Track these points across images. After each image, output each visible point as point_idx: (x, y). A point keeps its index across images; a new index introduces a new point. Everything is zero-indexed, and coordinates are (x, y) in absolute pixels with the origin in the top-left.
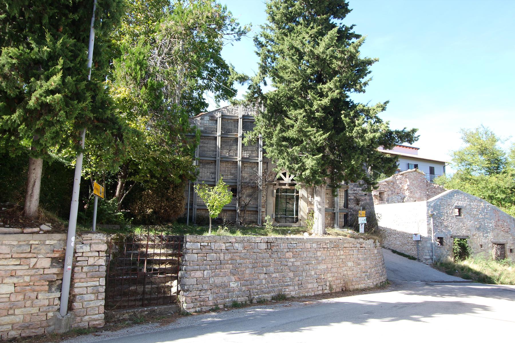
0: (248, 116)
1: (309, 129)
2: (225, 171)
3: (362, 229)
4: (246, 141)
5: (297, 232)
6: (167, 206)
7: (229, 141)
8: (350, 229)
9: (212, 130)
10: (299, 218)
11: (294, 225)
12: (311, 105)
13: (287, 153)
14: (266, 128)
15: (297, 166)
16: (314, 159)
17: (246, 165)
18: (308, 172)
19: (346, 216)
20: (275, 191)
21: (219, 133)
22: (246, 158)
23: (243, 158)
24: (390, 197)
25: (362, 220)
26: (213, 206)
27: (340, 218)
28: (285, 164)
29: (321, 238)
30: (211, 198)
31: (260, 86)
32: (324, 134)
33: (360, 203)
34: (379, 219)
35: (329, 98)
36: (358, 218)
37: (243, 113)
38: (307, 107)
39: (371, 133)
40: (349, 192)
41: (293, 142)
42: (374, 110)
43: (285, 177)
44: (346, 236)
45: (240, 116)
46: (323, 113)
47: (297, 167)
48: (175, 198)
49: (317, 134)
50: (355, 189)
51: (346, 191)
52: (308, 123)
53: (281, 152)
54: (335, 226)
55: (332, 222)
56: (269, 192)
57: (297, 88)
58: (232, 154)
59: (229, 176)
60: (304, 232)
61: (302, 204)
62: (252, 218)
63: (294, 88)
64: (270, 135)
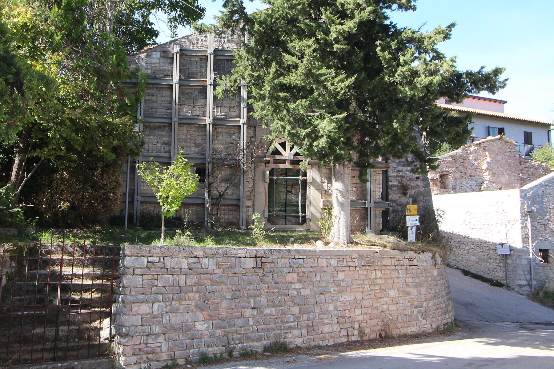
0: (223, 50)
1: (324, 70)
2: (185, 141)
3: (412, 236)
4: (220, 91)
5: (304, 240)
6: (93, 198)
7: (193, 92)
8: (393, 235)
9: (165, 73)
12: (327, 32)
13: (288, 110)
14: (252, 70)
15: (304, 132)
16: (333, 121)
17: (219, 130)
18: (322, 142)
19: (385, 214)
20: (268, 173)
21: (176, 79)
22: (220, 119)
24: (458, 182)
25: (412, 221)
26: (168, 197)
27: (375, 217)
29: (345, 249)
30: (164, 184)
32: (347, 78)
33: (409, 191)
34: (440, 219)
35: (356, 20)
36: (405, 216)
37: (215, 46)
38: (320, 35)
39: (426, 76)
40: (391, 174)
41: (297, 93)
42: (430, 38)
44: (385, 246)
45: (210, 51)
46: (347, 44)
47: (304, 133)
48: (106, 185)
49: (336, 80)
50: (399, 170)
51: (385, 173)
53: (277, 109)
54: (368, 230)
55: (362, 224)
57: (304, 4)
58: (197, 113)
59: (193, 149)
60: (316, 239)
61: (312, 192)
62: (230, 217)
64: (259, 82)
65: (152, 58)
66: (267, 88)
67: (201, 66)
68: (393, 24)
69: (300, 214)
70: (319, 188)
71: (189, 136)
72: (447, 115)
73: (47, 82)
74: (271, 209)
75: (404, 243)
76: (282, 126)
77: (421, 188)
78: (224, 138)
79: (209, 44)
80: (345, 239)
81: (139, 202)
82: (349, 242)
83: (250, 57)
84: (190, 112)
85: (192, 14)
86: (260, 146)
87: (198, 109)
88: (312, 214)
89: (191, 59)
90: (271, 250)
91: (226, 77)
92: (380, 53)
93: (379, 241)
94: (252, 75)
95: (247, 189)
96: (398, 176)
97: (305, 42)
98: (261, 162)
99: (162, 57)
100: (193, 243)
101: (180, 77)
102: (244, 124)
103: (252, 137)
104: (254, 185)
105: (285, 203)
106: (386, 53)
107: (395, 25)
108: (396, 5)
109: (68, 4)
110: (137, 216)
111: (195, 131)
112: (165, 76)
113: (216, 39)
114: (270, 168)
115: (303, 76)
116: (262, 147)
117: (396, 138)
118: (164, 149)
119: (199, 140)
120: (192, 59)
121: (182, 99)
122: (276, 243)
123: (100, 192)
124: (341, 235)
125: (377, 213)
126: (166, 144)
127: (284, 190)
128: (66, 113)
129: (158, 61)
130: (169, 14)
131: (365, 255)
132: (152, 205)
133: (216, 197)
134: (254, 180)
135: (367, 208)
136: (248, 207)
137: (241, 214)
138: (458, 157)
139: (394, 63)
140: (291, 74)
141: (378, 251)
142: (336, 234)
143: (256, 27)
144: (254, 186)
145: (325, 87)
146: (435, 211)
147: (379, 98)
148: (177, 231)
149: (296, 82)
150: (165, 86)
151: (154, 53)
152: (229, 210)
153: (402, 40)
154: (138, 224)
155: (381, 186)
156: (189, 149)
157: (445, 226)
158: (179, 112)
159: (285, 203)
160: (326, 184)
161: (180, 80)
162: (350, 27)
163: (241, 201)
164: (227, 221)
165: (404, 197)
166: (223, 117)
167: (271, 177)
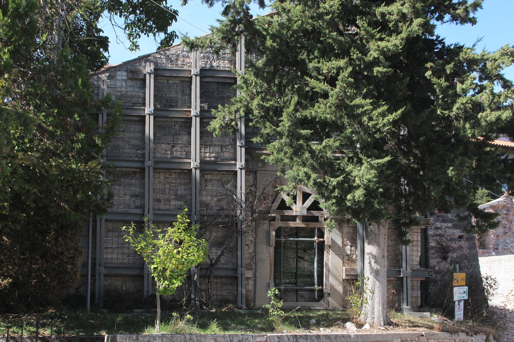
0: (212, 69)
2: (163, 192)
3: (459, 313)
4: (217, 126)
5: (327, 321)
6: (45, 271)
7: (171, 126)
8: (436, 312)
9: (134, 100)
10: (325, 291)
11: (316, 306)
12: (364, 51)
13: (312, 152)
14: (263, 99)
15: (334, 181)
17: (208, 177)
18: (359, 194)
19: (425, 285)
20: (274, 233)
21: (149, 109)
22: (210, 163)
23: (203, 162)
24: (501, 240)
25: (460, 293)
26: (165, 269)
27: (412, 289)
28: (309, 177)
29: (384, 333)
30: (160, 252)
31: (248, 9)
32: (390, 111)
33: (450, 255)
34: (491, 291)
35: (404, 35)
37: (201, 64)
38: (355, 54)
39: (492, 110)
40: (430, 232)
41: (322, 129)
42: (495, 60)
44: (431, 328)
45: (194, 71)
46: (389, 67)
47: (334, 183)
48: (62, 253)
49: (375, 113)
50: (445, 228)
51: (424, 232)
53: (297, 152)
54: (404, 306)
55: (396, 298)
56: (261, 235)
57: (333, 13)
58: (178, 154)
59: (173, 203)
60: (345, 321)
61: (331, 259)
62: (224, 293)
63: (327, 14)
64: (273, 114)
65: (116, 80)
66: (286, 123)
67: (183, 91)
68: (440, 39)
70: (340, 252)
72: (507, 156)
73: (25, 121)
74: (277, 281)
75: (452, 323)
76: (306, 173)
77: (465, 250)
78: (215, 188)
79: (194, 63)
80: (382, 319)
81: (102, 275)
82: (386, 323)
83: (259, 81)
84: (169, 152)
85: (159, 18)
86: (262, 197)
87: (179, 149)
89: (170, 83)
90: (296, 336)
91: (224, 107)
93: (421, 321)
94: (262, 105)
95: (246, 255)
100: (195, 330)
101: (154, 106)
103: (252, 186)
104: (255, 250)
105: (296, 273)
107: (442, 40)
108: (450, 16)
109: (16, 9)
111: (175, 179)
112: (134, 104)
114: (277, 227)
115: (333, 108)
116: (265, 199)
117: (449, 188)
118: (134, 202)
119: (181, 191)
120: (170, 82)
122: (299, 328)
124: (375, 314)
126: (137, 196)
128: (19, 157)
129: (124, 84)
130: (127, 18)
131: (409, 339)
132: (119, 278)
133: (205, 266)
135: (402, 278)
136: (248, 278)
137: (240, 288)
138: (500, 208)
141: (423, 333)
142: (369, 313)
143: (269, 43)
144: (255, 251)
145: (361, 123)
146: (484, 279)
148: (174, 314)
149: (325, 115)
151: (119, 73)
153: (461, 63)
154: (102, 305)
155: (419, 249)
156: (168, 203)
157: (495, 301)
158: (154, 153)
159: (296, 273)
160: (349, 247)
161: (155, 110)
162: (395, 45)
163: (239, 272)
165: (444, 262)
166: (213, 159)
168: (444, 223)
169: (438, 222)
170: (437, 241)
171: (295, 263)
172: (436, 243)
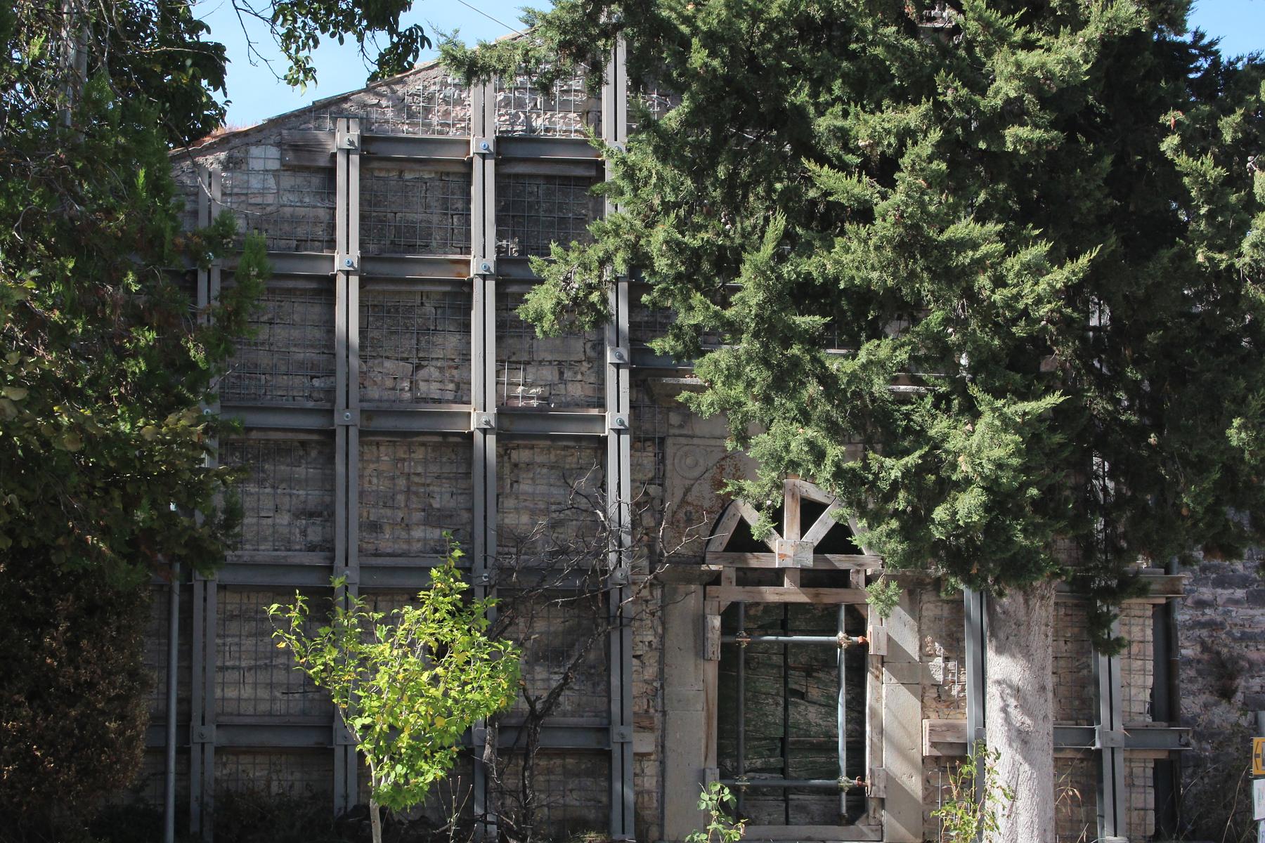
0: (530, 138)
1: (964, 227)
2: (388, 501)
4: (548, 305)
7: (414, 304)
9: (301, 231)
10: (871, 792)
12: (978, 80)
13: (828, 380)
14: (681, 226)
15: (895, 468)
16: (1007, 424)
17: (522, 456)
18: (969, 504)
19: (1166, 775)
20: (717, 622)
21: (346, 256)
22: (526, 414)
23: (504, 412)
26: (394, 731)
27: (1130, 785)
30: (382, 680)
32: (1056, 258)
33: (1241, 682)
35: (1093, 31)
36: (1248, 784)
37: (497, 122)
40: (1182, 616)
43: (804, 528)
45: (479, 143)
46: (1053, 125)
48: (91, 685)
49: (1013, 264)
51: (1164, 614)
52: (953, 192)
53: (784, 379)
56: (680, 632)
58: (433, 390)
59: (418, 533)
61: (886, 696)
62: (573, 800)
65: (249, 172)
66: (749, 294)
67: (445, 201)
68: (1205, 41)
69: (844, 780)
70: (913, 676)
71: (402, 483)
74: (728, 763)
76: (811, 443)
78: (541, 489)
81: (209, 751)
83: (669, 172)
84: (406, 385)
86: (681, 515)
87: (436, 374)
88: (890, 780)
91: (567, 249)
92: (1183, 161)
94: (678, 244)
96: (1198, 624)
97: (893, 118)
98: (689, 582)
99: (287, 168)
102: (619, 432)
104: (661, 671)
105: (783, 740)
106: (1208, 160)
107: (1212, 43)
110: (203, 805)
111: (425, 462)
112: (302, 243)
113: (501, 96)
114: (725, 603)
115: (889, 253)
116: (689, 521)
118: (304, 533)
119: (442, 498)
120: (408, 176)
121: (374, 334)
123: (66, 715)
125: (1137, 771)
126: (311, 515)
127: (779, 686)
129: (271, 182)
132: (259, 759)
133: (513, 721)
134: (662, 651)
135: (1099, 752)
136: (641, 756)
137: (617, 786)
139: (1233, 198)
140: (839, 241)
143: (698, 57)
145: (971, 295)
147: (1166, 329)
149: (863, 273)
150: (301, 284)
151: (255, 151)
152: (567, 773)
155: (1150, 666)
156: (404, 534)
158: (363, 386)
159: (783, 740)
160: (939, 661)
161: (362, 259)
162: (1069, 61)
163: (616, 738)
164: (558, 814)
166: (534, 403)
167: (729, 639)
168: (1224, 588)
169: (1205, 585)
170: (1203, 643)
171: (780, 709)
172: (1198, 648)
